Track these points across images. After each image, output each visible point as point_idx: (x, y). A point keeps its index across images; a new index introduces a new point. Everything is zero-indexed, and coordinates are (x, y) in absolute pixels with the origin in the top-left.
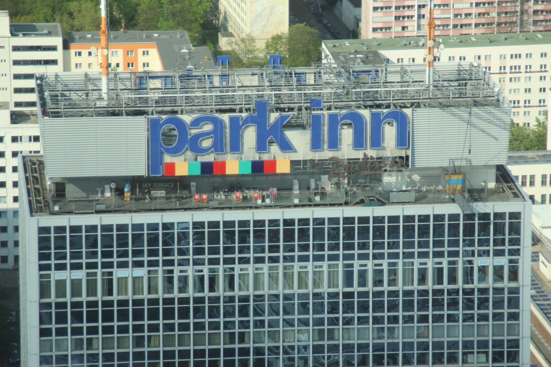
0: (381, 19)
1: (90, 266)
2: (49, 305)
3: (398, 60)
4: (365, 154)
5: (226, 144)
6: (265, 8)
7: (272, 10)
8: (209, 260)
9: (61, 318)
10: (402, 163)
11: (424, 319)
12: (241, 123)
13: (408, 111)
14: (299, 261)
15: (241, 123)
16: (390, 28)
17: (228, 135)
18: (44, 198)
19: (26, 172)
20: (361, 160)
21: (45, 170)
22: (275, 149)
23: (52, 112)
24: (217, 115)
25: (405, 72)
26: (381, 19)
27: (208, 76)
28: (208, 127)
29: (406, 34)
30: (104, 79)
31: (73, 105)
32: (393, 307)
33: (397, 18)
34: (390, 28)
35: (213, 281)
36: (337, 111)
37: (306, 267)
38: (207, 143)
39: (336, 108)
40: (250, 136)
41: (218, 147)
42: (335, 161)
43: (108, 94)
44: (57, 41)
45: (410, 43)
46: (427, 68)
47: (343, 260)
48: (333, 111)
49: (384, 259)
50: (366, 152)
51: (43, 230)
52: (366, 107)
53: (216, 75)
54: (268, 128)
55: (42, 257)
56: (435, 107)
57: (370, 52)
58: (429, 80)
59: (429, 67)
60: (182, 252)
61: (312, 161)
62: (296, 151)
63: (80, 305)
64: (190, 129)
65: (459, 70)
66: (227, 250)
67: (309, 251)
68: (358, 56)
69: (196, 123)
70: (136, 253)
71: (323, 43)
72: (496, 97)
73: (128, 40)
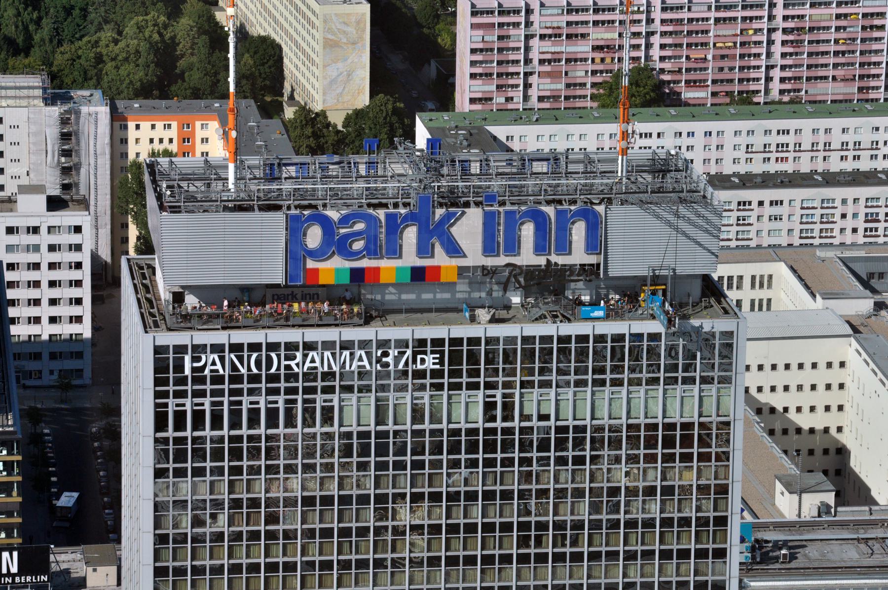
0: (480, 88)
1: (506, 385)
2: (166, 441)
3: (508, 137)
4: (548, 260)
5: (381, 246)
6: (341, 74)
7: (349, 75)
8: (432, 385)
9: (180, 456)
10: (590, 272)
11: (473, 464)
12: (399, 221)
13: (601, 209)
14: (467, 389)
15: (399, 221)
16: (491, 99)
18: (158, 310)
19: (133, 278)
20: (543, 267)
22: (438, 249)
23: (170, 207)
24: (371, 211)
25: (591, 162)
26: (480, 88)
27: (355, 163)
28: (360, 226)
29: (510, 106)
30: (231, 167)
31: (191, 198)
33: (499, 87)
34: (491, 99)
36: (515, 208)
37: (331, 401)
38: (358, 245)
39: (512, 204)
40: (410, 236)
41: (372, 251)
43: (235, 184)
45: (521, 118)
46: (620, 157)
47: (229, 396)
48: (508, 207)
49: (205, 396)
50: (549, 257)
51: (159, 350)
52: (549, 203)
53: (119, 142)
54: (431, 227)
55: (158, 382)
56: (632, 204)
57: (474, 128)
58: (622, 171)
59: (623, 155)
60: (470, 374)
61: (484, 268)
62: (465, 256)
63: (239, 439)
64: (338, 228)
65: (653, 160)
66: (542, 371)
67: (187, 385)
68: (460, 132)
69: (345, 220)
70: (542, 371)
71: (418, 120)
72: (702, 193)
73: (183, 111)
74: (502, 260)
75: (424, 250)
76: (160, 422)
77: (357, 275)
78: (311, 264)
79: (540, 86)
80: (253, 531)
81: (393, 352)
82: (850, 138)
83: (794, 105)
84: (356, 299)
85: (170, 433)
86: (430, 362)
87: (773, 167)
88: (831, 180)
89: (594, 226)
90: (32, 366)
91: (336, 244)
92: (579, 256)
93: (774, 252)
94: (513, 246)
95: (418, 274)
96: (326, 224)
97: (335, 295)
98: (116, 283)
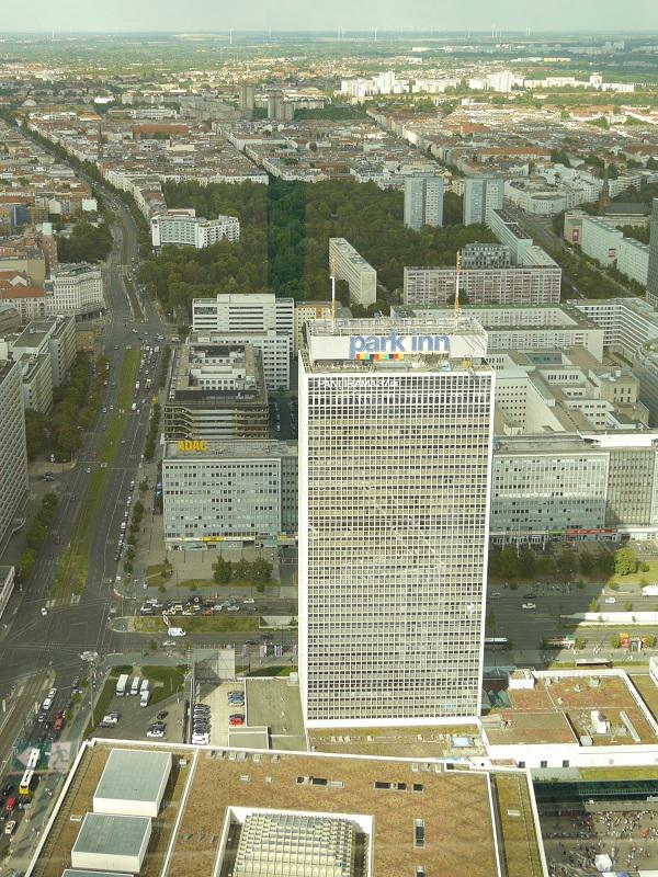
10: (446, 357)
13: (449, 336)
17: (555, 60)
21: (220, 663)
28: (373, 341)
32: (471, 411)
35: (374, 400)
38: (372, 347)
40: (388, 344)
41: (377, 348)
42: (421, 355)
44: (293, 305)
74: (417, 352)
75: (393, 348)
76: (311, 402)
77: (372, 356)
78: (357, 353)
79: (431, 297)
80: (623, 451)
81: (383, 381)
82: (528, 315)
83: (511, 305)
84: (366, 364)
85: (313, 405)
86: (395, 384)
87: (504, 324)
88: (522, 328)
89: (447, 341)
90: (272, 384)
91: (365, 346)
92: (442, 351)
93: (504, 351)
94: (421, 348)
95: (391, 356)
96: (362, 340)
97: (364, 363)
98: (297, 359)
